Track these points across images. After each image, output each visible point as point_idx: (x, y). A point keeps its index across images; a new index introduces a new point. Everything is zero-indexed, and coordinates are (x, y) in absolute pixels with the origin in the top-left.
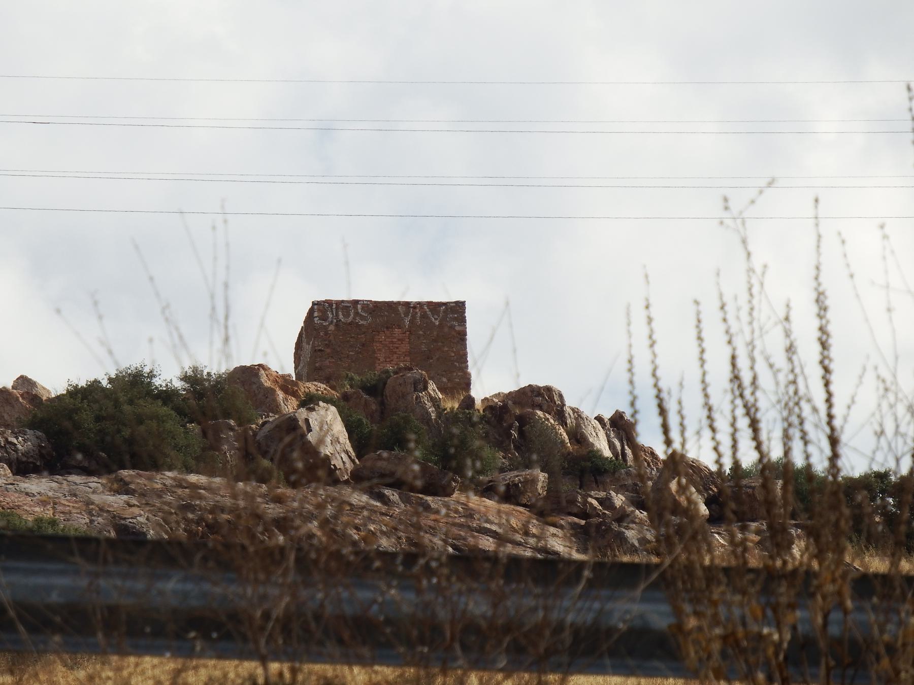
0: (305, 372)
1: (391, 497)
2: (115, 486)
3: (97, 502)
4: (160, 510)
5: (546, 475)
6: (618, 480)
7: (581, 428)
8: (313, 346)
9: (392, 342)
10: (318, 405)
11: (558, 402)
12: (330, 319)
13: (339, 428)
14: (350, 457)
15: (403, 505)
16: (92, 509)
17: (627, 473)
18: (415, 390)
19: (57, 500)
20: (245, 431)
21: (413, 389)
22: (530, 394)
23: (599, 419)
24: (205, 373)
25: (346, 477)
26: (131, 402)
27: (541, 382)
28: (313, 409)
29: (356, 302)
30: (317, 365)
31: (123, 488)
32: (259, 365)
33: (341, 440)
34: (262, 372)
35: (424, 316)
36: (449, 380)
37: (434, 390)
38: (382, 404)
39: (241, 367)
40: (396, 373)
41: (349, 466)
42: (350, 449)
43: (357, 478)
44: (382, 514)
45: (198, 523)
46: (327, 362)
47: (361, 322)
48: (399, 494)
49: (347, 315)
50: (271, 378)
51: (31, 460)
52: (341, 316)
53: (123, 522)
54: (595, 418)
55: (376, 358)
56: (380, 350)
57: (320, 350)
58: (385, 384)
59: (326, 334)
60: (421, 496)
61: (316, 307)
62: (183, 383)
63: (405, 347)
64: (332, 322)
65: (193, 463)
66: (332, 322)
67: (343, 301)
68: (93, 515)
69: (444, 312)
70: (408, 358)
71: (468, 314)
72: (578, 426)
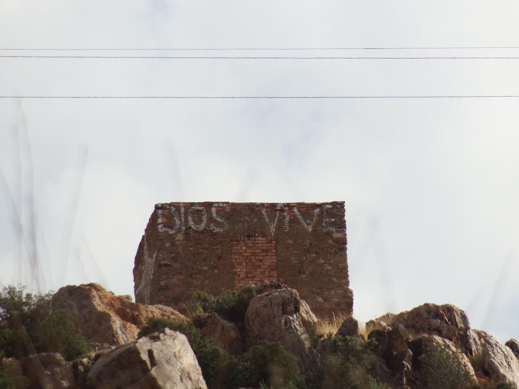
9: (254, 254)
10: (164, 332)
11: (461, 325)
12: (177, 227)
18: (285, 312)
20: (75, 367)
21: (281, 312)
22: (425, 315)
24: (24, 295)
27: (439, 300)
29: (209, 205)
33: (192, 376)
34: (95, 293)
35: (294, 221)
36: (325, 300)
37: (307, 313)
38: (242, 330)
46: (175, 280)
47: (217, 230)
49: (198, 221)
50: (106, 301)
52: (191, 223)
54: (507, 344)
55: (235, 273)
56: (240, 264)
57: (166, 265)
58: (246, 305)
59: (173, 244)
61: (160, 211)
66: (179, 230)
67: (193, 204)
69: (319, 216)
70: (275, 274)
72: (486, 354)
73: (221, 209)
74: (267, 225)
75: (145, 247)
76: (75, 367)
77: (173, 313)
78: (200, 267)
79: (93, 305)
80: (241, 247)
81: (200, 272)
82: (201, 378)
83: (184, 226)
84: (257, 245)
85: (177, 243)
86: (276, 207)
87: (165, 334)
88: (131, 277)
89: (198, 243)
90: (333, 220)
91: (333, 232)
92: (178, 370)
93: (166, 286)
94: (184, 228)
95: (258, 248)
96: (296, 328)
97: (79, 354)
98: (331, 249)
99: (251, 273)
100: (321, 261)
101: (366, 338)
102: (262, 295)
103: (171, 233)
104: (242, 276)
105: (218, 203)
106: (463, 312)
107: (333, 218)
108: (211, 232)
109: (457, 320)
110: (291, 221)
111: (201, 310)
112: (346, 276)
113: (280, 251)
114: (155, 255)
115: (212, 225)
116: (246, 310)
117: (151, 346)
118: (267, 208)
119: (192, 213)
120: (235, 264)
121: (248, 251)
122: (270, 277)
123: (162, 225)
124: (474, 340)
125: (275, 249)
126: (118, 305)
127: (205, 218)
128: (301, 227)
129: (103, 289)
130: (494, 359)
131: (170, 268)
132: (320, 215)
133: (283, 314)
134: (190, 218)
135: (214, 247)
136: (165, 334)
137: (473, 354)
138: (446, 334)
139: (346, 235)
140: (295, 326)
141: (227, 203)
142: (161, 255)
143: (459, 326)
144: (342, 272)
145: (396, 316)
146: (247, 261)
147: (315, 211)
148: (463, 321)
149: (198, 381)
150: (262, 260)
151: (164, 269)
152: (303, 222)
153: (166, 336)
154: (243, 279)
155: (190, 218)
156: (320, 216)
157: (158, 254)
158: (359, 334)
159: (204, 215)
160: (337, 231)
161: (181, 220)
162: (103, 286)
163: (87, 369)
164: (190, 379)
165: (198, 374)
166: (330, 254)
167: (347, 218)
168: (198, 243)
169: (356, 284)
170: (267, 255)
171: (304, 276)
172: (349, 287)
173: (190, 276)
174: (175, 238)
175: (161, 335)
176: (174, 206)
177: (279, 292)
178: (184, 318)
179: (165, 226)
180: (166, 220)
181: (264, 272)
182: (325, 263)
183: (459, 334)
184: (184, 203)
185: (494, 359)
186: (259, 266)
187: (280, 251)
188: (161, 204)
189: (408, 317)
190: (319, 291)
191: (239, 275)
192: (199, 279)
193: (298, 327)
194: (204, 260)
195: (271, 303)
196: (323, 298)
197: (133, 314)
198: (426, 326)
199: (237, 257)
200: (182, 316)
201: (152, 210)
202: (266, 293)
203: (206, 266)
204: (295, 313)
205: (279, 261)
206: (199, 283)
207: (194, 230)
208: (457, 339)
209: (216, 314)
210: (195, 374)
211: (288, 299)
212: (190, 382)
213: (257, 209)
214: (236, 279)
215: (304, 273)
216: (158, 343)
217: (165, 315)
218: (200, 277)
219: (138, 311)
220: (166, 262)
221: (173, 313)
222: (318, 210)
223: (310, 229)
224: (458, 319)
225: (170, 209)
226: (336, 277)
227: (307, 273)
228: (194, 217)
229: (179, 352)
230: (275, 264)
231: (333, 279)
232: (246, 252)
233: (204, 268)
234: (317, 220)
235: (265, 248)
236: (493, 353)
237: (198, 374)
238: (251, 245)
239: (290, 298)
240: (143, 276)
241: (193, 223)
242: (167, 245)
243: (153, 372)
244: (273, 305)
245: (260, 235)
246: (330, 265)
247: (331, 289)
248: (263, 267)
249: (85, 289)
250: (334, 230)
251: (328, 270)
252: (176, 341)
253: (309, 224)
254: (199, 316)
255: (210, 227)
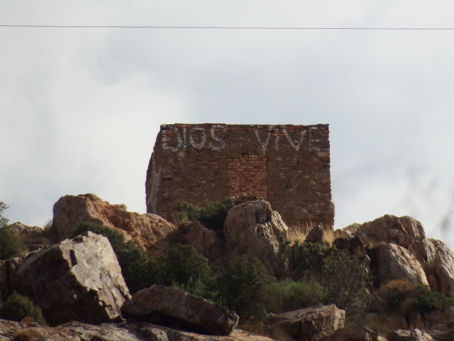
0: (154, 205)
8: (162, 175)
9: (247, 170)
10: (86, 235)
11: (417, 234)
12: (180, 145)
14: (122, 293)
18: (258, 221)
20: (8, 265)
21: (254, 221)
22: (385, 225)
25: (117, 315)
27: (399, 213)
28: (81, 240)
29: (208, 126)
30: (166, 195)
33: (112, 274)
34: (89, 202)
36: (310, 211)
37: (279, 222)
38: (221, 237)
39: (61, 199)
40: (237, 202)
41: (120, 302)
42: (122, 283)
43: (130, 317)
46: (176, 192)
47: (215, 148)
49: (199, 141)
50: (100, 209)
52: (192, 142)
55: (230, 187)
56: (234, 178)
57: (168, 179)
58: (225, 215)
59: (176, 161)
60: (192, 335)
61: (164, 132)
66: (182, 149)
69: (305, 137)
70: (265, 188)
72: (437, 260)
73: (219, 130)
74: (260, 145)
75: (154, 163)
76: (8, 265)
78: (199, 181)
79: (88, 213)
80: (236, 163)
81: (199, 186)
82: (121, 276)
83: (186, 144)
84: (250, 162)
85: (179, 159)
86: (268, 128)
87: (88, 237)
89: (198, 160)
90: (318, 141)
91: (318, 151)
92: (99, 269)
93: (169, 197)
94: (185, 147)
95: (251, 164)
96: (267, 236)
98: (316, 166)
99: (244, 187)
100: (307, 177)
101: (331, 245)
102: (239, 205)
103: (174, 150)
104: (236, 189)
105: (217, 124)
106: (419, 223)
107: (318, 139)
108: (210, 150)
109: (414, 230)
110: (281, 142)
111: (186, 218)
112: (329, 190)
113: (270, 168)
114: (160, 170)
115: (210, 145)
116: (225, 219)
117: (73, 247)
118: (259, 129)
119: (193, 133)
120: (230, 178)
121: (242, 167)
122: (261, 190)
123: (166, 144)
124: (430, 248)
125: (266, 166)
126: (111, 213)
127: (204, 138)
128: (289, 147)
129: (98, 199)
130: (444, 265)
131: (172, 181)
132: (307, 137)
133: (257, 222)
134: (191, 138)
135: (212, 164)
136: (88, 237)
137: (428, 260)
138: (403, 243)
139: (329, 154)
140: (266, 234)
142: (164, 170)
143: (415, 235)
144: (325, 188)
145: (360, 226)
146: (241, 176)
147: (302, 132)
148: (419, 231)
149: (117, 278)
150: (255, 175)
152: (291, 142)
153: (88, 239)
154: (237, 192)
155: (191, 138)
156: (307, 137)
157: (162, 170)
158: (324, 241)
159: (204, 135)
160: (322, 151)
161: (183, 139)
162: (99, 196)
163: (18, 266)
164: (110, 276)
165: (118, 272)
166: (315, 170)
167: (331, 138)
168: (198, 160)
169: (336, 198)
170: (259, 171)
171: (291, 190)
172: (332, 201)
173: (190, 188)
174: (178, 155)
175: (84, 238)
176: (178, 127)
177: (253, 203)
178: (171, 226)
180: (169, 139)
181: (256, 186)
182: (310, 178)
183: (415, 243)
184: (186, 124)
185: (444, 265)
186: (252, 180)
187: (270, 168)
188: (166, 125)
189: (370, 227)
190: (304, 203)
191: (233, 189)
192: (198, 191)
193: (269, 234)
194: (203, 174)
195: (246, 213)
196: (307, 209)
197: (124, 221)
198: (386, 235)
199: (232, 173)
200: (169, 224)
201: (158, 130)
202: (242, 204)
203: (204, 180)
204: (267, 222)
205: (269, 176)
206: (198, 195)
207: (194, 149)
208: (413, 247)
209: (199, 222)
210: (115, 272)
211: (261, 210)
212: (109, 279)
213: (251, 130)
214: (231, 192)
215: (291, 187)
216: (81, 244)
217: (154, 222)
218: (199, 189)
219: (129, 219)
220: (169, 176)
221: (160, 221)
222: (305, 131)
223: (298, 148)
224: (414, 229)
225: (173, 129)
226: (320, 192)
227: (294, 187)
228: (195, 137)
229: (101, 252)
230: (265, 179)
231: (317, 193)
232: (240, 168)
233: (202, 182)
234: (303, 140)
235: (258, 165)
236: (444, 260)
237: (118, 272)
238: (245, 162)
239: (263, 209)
240: (152, 188)
241: (194, 142)
242: (171, 161)
243: (74, 270)
244: (248, 214)
245: (253, 153)
246: (315, 181)
247: (316, 202)
248: (255, 181)
249: (82, 198)
250: (319, 150)
251: (312, 185)
252: (98, 243)
253: (296, 144)
254: (183, 224)
255: (208, 146)
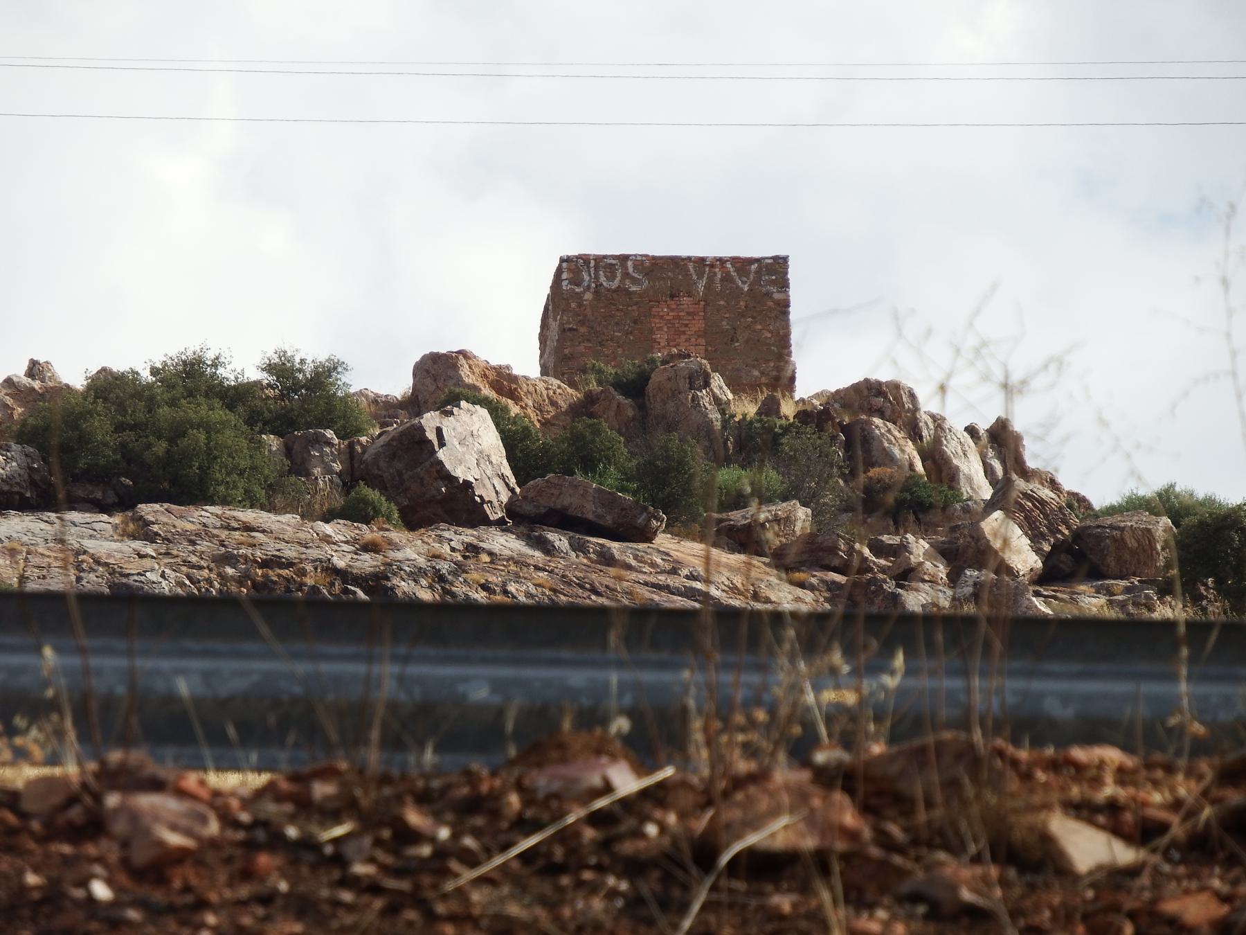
1: (557, 544)
2: (131, 527)
3: (91, 551)
4: (186, 563)
5: (809, 511)
6: (950, 519)
7: (941, 442)
8: (561, 324)
9: (679, 318)
10: (458, 406)
11: (908, 405)
13: (490, 439)
14: (507, 485)
15: (573, 555)
16: (82, 561)
17: (963, 508)
19: (32, 548)
20: (351, 447)
22: (865, 392)
23: (972, 431)
24: (297, 360)
26: (173, 403)
29: (624, 258)
30: (566, 351)
31: (144, 531)
32: (460, 352)
33: (494, 459)
34: (462, 361)
35: (727, 278)
36: (762, 373)
38: (642, 408)
39: (431, 354)
40: (664, 362)
41: (505, 497)
42: (508, 472)
44: (537, 568)
45: (240, 582)
46: (581, 348)
47: (634, 288)
48: (570, 539)
49: (611, 278)
51: (16, 489)
52: (602, 279)
53: (124, 580)
54: (966, 429)
55: (655, 341)
56: (660, 329)
57: (571, 330)
59: (580, 305)
61: (565, 265)
62: (265, 375)
63: (698, 324)
64: (589, 286)
65: (261, 494)
66: (589, 286)
67: (605, 257)
68: (84, 570)
69: (756, 272)
70: (702, 341)
71: (792, 275)
72: (937, 441)
76: (351, 447)
77: (559, 387)
82: (505, 461)
88: (536, 344)
97: (359, 431)
100: (759, 327)
108: (626, 290)
115: (627, 282)
126: (492, 375)
132: (758, 272)
141: (647, 256)
151: (569, 334)
164: (491, 463)
175: (455, 410)
179: (570, 283)
194: (617, 324)
209: (611, 388)
221: (559, 387)
243: (441, 454)
